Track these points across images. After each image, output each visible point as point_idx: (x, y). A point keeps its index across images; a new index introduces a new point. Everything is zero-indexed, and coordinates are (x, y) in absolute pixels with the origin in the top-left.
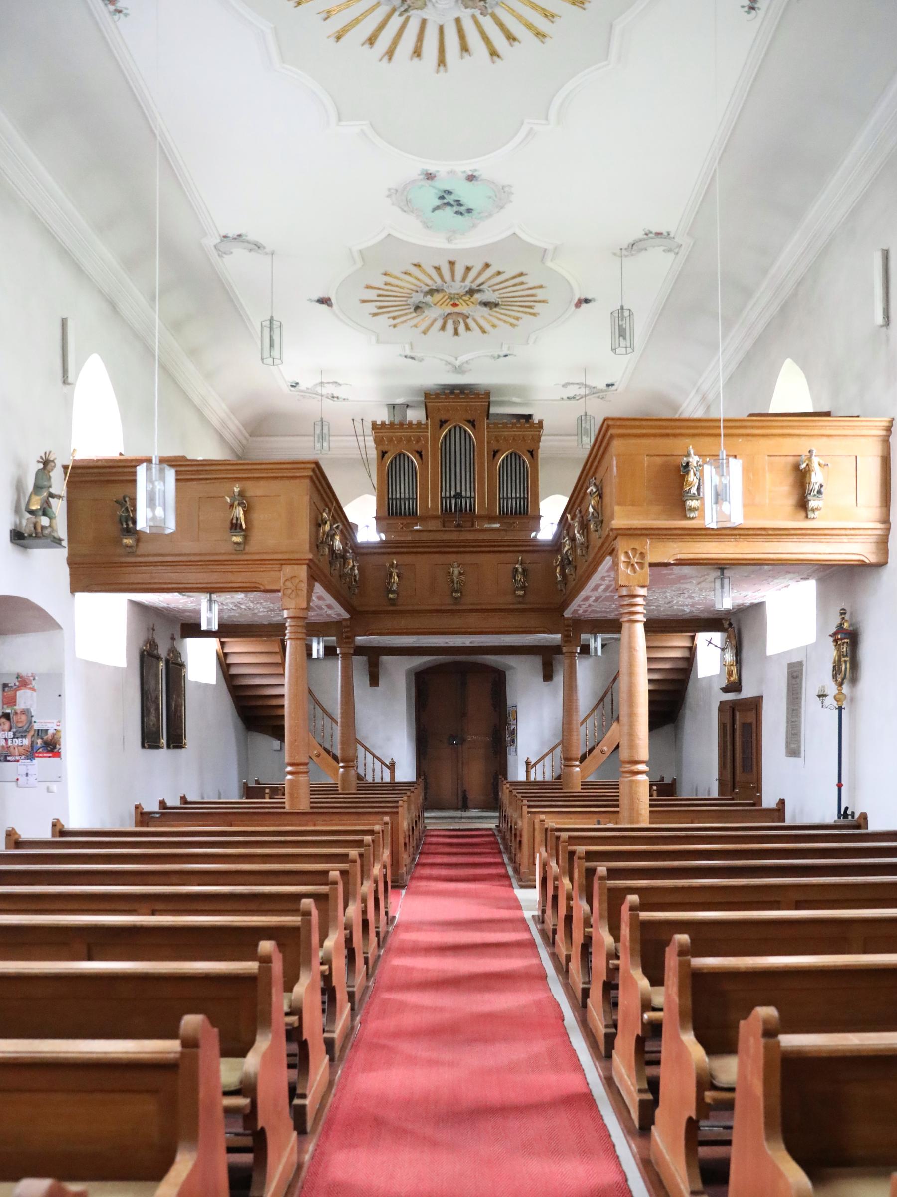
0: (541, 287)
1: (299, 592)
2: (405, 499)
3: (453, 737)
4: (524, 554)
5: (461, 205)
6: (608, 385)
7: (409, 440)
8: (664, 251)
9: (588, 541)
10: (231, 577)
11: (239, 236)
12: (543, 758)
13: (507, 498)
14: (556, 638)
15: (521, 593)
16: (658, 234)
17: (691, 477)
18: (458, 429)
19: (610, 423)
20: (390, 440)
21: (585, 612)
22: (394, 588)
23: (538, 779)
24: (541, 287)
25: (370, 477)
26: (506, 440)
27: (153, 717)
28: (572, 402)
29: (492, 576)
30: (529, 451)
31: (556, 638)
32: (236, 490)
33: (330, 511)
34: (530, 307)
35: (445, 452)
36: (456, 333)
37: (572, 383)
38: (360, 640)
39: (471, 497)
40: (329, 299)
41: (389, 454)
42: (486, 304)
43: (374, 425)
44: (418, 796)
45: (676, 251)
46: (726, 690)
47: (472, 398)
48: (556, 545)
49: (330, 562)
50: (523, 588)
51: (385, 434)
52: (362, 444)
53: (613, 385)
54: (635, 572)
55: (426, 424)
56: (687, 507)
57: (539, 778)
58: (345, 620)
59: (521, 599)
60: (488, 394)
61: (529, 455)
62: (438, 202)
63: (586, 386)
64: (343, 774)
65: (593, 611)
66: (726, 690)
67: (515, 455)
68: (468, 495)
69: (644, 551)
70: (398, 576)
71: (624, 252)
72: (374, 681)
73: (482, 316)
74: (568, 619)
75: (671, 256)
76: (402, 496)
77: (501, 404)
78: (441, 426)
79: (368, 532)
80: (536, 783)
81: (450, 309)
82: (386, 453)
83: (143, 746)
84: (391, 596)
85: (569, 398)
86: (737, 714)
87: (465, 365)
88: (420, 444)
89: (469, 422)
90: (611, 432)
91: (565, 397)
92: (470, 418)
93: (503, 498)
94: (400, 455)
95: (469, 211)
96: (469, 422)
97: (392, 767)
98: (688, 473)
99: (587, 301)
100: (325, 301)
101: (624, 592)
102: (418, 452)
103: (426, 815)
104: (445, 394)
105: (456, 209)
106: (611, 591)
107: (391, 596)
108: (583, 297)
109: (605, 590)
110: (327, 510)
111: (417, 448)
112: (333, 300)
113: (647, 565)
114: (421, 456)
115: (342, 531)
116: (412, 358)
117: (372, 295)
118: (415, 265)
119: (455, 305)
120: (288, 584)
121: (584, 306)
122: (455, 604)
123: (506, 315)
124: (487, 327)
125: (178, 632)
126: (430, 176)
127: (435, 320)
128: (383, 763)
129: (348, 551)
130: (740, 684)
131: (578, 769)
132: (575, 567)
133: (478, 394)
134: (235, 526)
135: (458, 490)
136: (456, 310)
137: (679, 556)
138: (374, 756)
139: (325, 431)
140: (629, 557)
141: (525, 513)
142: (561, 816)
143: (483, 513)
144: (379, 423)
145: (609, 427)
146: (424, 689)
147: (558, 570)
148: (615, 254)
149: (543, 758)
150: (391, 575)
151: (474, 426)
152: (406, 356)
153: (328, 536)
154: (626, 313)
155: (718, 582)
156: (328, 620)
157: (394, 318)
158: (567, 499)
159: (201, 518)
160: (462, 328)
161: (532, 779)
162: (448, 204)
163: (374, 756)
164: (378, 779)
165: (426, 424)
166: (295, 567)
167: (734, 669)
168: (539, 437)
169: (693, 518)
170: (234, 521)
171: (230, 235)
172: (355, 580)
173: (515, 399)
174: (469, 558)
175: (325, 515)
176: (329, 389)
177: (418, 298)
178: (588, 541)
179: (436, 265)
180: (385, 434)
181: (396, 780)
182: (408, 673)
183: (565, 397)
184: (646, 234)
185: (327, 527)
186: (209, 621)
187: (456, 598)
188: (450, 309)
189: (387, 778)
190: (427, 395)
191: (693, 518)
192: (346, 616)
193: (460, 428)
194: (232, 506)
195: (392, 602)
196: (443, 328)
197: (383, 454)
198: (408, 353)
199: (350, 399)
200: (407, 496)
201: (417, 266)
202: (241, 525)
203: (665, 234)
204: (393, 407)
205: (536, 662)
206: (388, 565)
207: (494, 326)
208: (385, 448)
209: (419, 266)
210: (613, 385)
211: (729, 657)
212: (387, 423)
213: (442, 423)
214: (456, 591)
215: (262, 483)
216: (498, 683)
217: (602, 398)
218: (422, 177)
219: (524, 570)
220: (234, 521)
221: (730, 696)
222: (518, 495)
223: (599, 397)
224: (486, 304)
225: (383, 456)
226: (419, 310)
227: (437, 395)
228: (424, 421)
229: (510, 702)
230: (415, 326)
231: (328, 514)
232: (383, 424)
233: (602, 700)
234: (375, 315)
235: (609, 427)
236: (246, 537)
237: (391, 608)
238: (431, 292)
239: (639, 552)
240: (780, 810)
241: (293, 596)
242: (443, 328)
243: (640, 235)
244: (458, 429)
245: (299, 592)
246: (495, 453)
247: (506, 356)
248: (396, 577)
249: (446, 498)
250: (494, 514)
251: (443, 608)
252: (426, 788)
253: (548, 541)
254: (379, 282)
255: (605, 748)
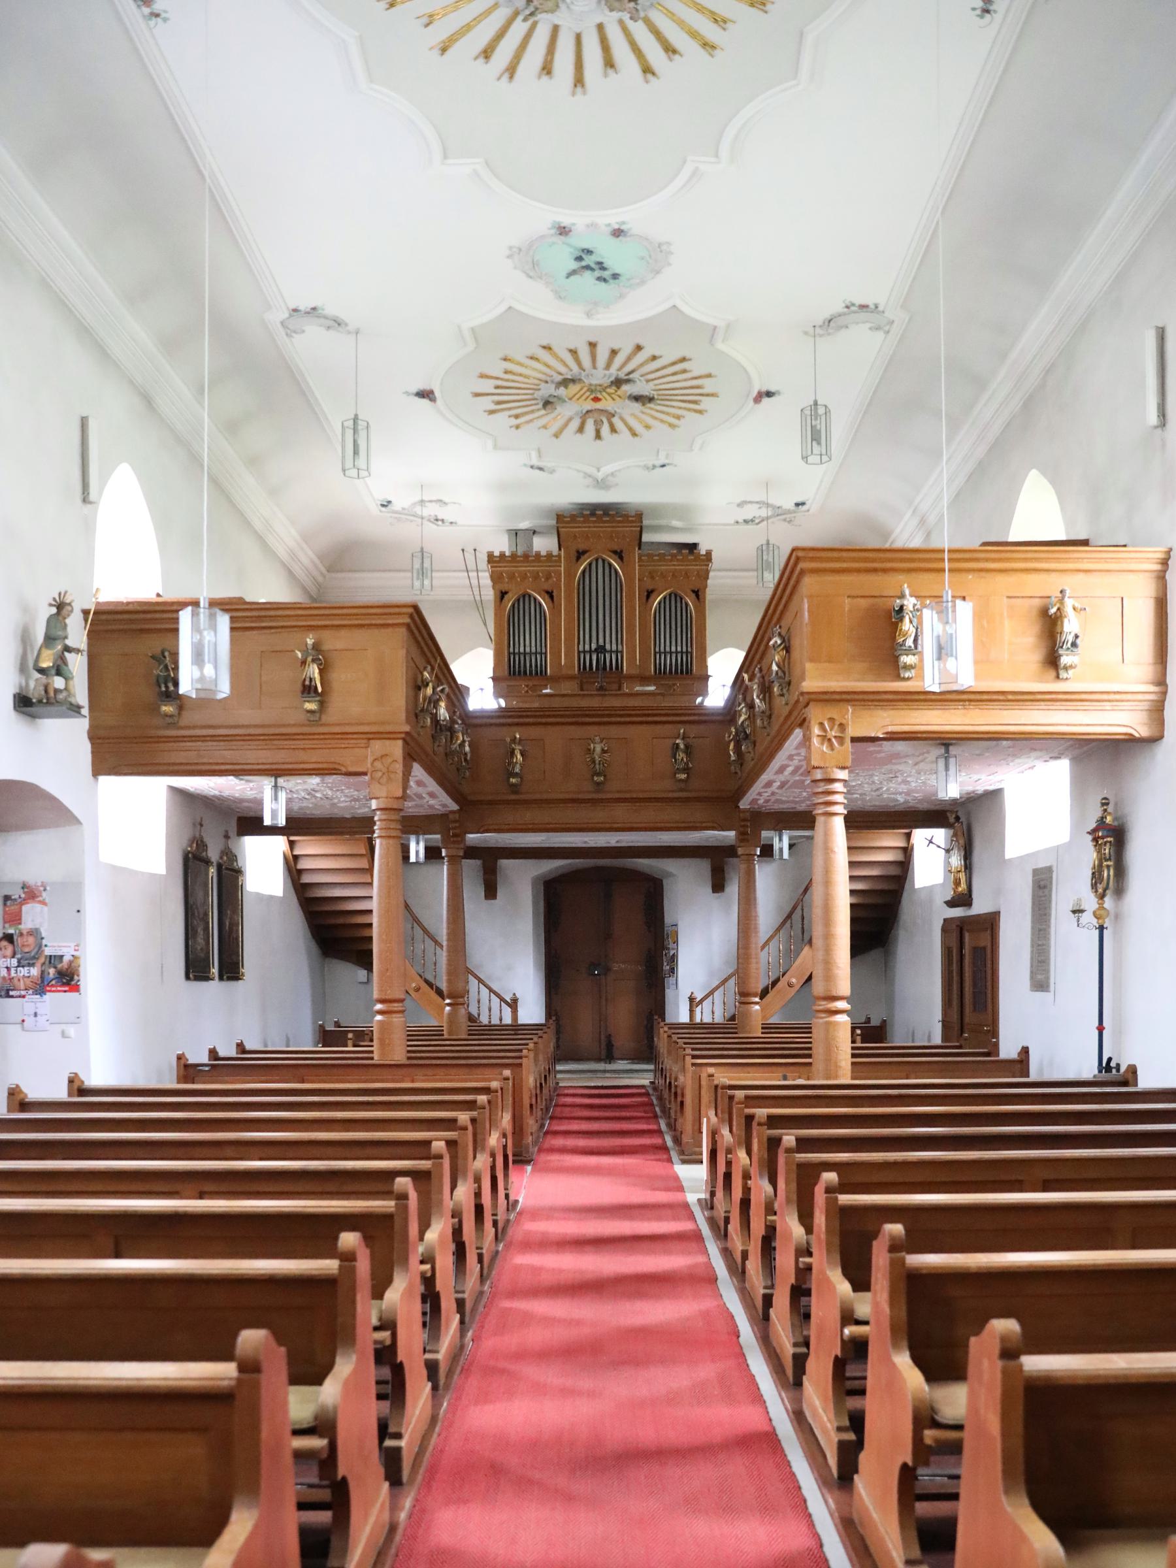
0: (709, 376)
1: (392, 776)
2: (531, 653)
3: (594, 965)
4: (688, 726)
5: (604, 269)
6: (797, 505)
7: (536, 577)
8: (870, 329)
9: (770, 709)
10: (302, 756)
11: (314, 309)
12: (711, 993)
13: (665, 653)
14: (729, 836)
15: (683, 776)
16: (863, 307)
17: (906, 625)
18: (600, 562)
19: (800, 554)
20: (512, 577)
21: (767, 801)
22: (517, 770)
23: (705, 1021)
24: (709, 376)
25: (485, 624)
26: (663, 576)
27: (200, 940)
28: (750, 527)
29: (645, 755)
30: (693, 591)
31: (729, 836)
32: (310, 642)
33: (433, 669)
34: (695, 402)
35: (583, 592)
36: (598, 436)
37: (751, 502)
38: (472, 838)
39: (617, 652)
40: (432, 392)
41: (510, 595)
42: (637, 398)
43: (490, 556)
44: (548, 1043)
45: (887, 328)
46: (951, 904)
47: (619, 522)
48: (728, 714)
49: (433, 736)
50: (686, 770)
51: (505, 569)
52: (474, 582)
53: (803, 504)
54: (832, 749)
55: (559, 556)
56: (901, 664)
57: (707, 1019)
58: (453, 812)
59: (683, 785)
60: (639, 516)
61: (693, 596)
62: (574, 265)
63: (768, 505)
64: (450, 1014)
65: (777, 801)
66: (951, 904)
67: (676, 596)
68: (614, 648)
69: (844, 722)
70: (522, 755)
71: (818, 331)
72: (491, 892)
73: (632, 415)
74: (745, 811)
75: (880, 335)
76: (528, 650)
77: (657, 529)
78: (578, 558)
79: (483, 696)
80: (702, 1026)
81: (590, 405)
82: (506, 593)
83: (187, 978)
84: (513, 780)
85: (746, 521)
86: (967, 935)
87: (610, 478)
88: (550, 581)
89: (615, 552)
90: (801, 565)
91: (741, 520)
92: (616, 548)
93: (660, 653)
94: (524, 596)
95: (615, 276)
96: (615, 552)
97: (514, 1004)
98: (901, 619)
99: (769, 394)
100: (426, 394)
101: (818, 775)
102: (547, 592)
103: (559, 1068)
104: (583, 516)
105: (598, 273)
106: (802, 775)
107: (513, 780)
108: (764, 389)
109: (794, 772)
110: (429, 668)
111: (547, 587)
112: (437, 394)
113: (848, 740)
114: (552, 597)
115: (448, 696)
116: (541, 469)
117: (487, 386)
118: (544, 347)
119: (596, 400)
120: (378, 765)
121: (766, 400)
122: (597, 791)
123: (663, 412)
124: (638, 428)
125: (233, 828)
126: (563, 231)
127: (570, 419)
128: (502, 999)
129: (456, 722)
130: (970, 896)
131: (757, 1007)
132: (754, 743)
133: (627, 516)
134: (308, 689)
135: (601, 642)
136: (598, 405)
137: (890, 729)
138: (491, 990)
139: (427, 564)
140: (825, 730)
141: (689, 671)
142: (735, 1069)
143: (634, 672)
144: (497, 554)
145: (798, 559)
146: (556, 902)
147: (731, 747)
148: (806, 333)
149: (711, 993)
150: (512, 753)
151: (621, 558)
152: (532, 467)
153: (430, 702)
154: (821, 411)
155: (941, 763)
156: (430, 812)
157: (517, 417)
158: (744, 654)
159: (264, 678)
160: (605, 430)
161: (698, 1020)
162: (588, 267)
163: (491, 990)
164: (495, 1021)
165: (559, 556)
166: (387, 742)
167: (962, 876)
168: (707, 572)
169: (909, 679)
170: (307, 683)
171: (302, 308)
172: (466, 760)
173: (676, 523)
174: (614, 731)
175: (426, 674)
176: (431, 510)
177: (548, 390)
178: (770, 709)
179: (572, 347)
180: (505, 569)
181: (520, 1022)
182: (535, 881)
183: (741, 520)
184: (847, 307)
185: (429, 691)
186: (274, 814)
187: (598, 784)
188: (590, 405)
189: (508, 1020)
190: (560, 517)
191: (909, 679)
192: (454, 807)
193: (604, 561)
194: (304, 663)
195: (515, 789)
196: (581, 430)
197: (502, 595)
198: (535, 462)
199: (459, 523)
200: (533, 650)
201: (547, 348)
202: (316, 687)
203: (872, 307)
204: (515, 533)
205: (703, 867)
206: (508, 740)
207: (648, 427)
208: (505, 587)
209: (550, 349)
210: (803, 504)
211: (956, 861)
212: (507, 554)
213: (580, 555)
214: (598, 774)
215: (343, 633)
216: (652, 895)
217: (790, 522)
218: (553, 231)
219: (687, 747)
220: (307, 683)
221: (958, 912)
222: (679, 649)
223: (785, 520)
224: (637, 398)
225: (502, 598)
226: (549, 406)
227: (573, 518)
228: (555, 552)
229: (668, 920)
230: (545, 427)
231: (430, 674)
232: (502, 555)
233: (789, 916)
234: (492, 412)
235: (798, 559)
236: (322, 704)
237: (513, 797)
238: (565, 383)
239: (837, 723)
240: (1023, 1060)
241: (384, 780)
242: (581, 430)
243: (839, 308)
244: (600, 562)
245: (392, 776)
246: (649, 594)
247: (663, 466)
248: (519, 756)
249: (584, 652)
250: (647, 674)
251: (581, 796)
252: (558, 1032)
253: (718, 709)
254: (497, 369)
255: (794, 980)
